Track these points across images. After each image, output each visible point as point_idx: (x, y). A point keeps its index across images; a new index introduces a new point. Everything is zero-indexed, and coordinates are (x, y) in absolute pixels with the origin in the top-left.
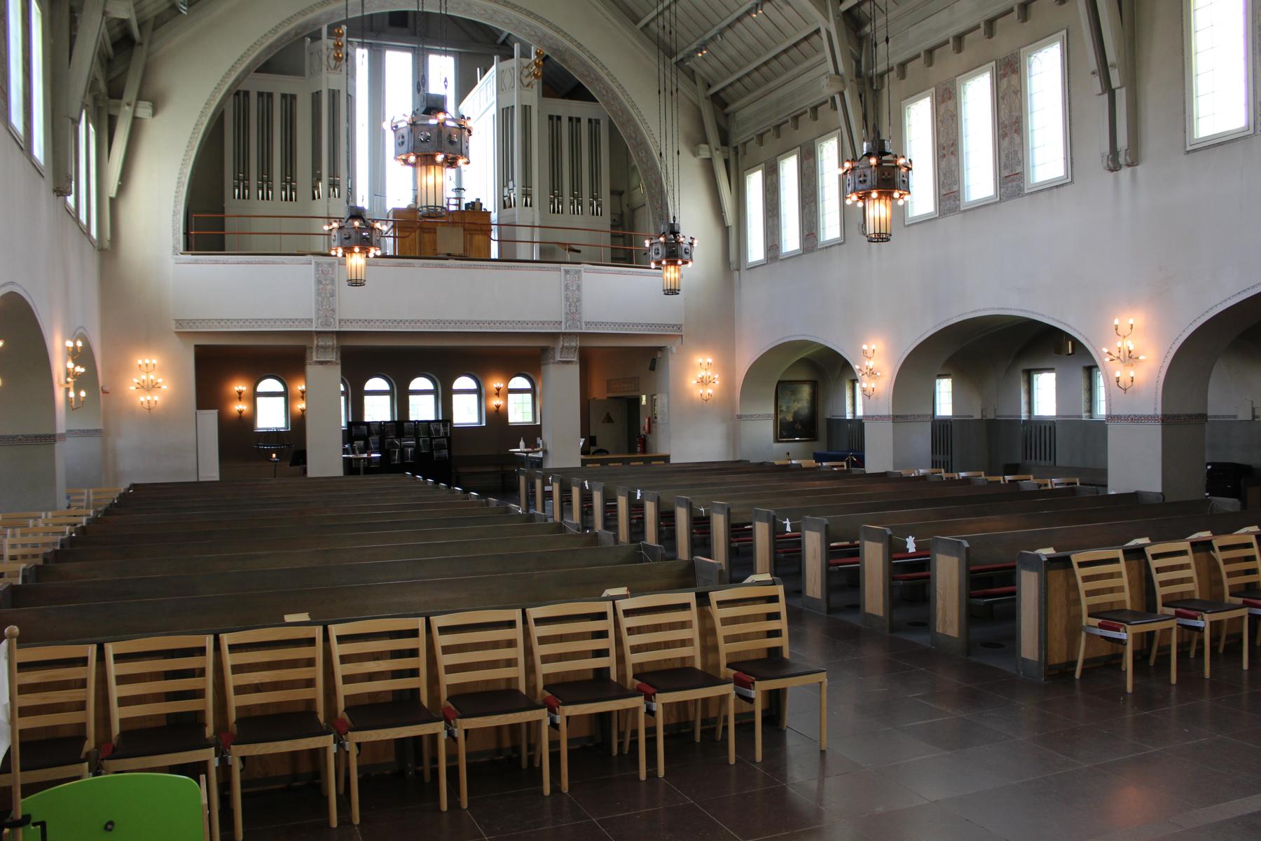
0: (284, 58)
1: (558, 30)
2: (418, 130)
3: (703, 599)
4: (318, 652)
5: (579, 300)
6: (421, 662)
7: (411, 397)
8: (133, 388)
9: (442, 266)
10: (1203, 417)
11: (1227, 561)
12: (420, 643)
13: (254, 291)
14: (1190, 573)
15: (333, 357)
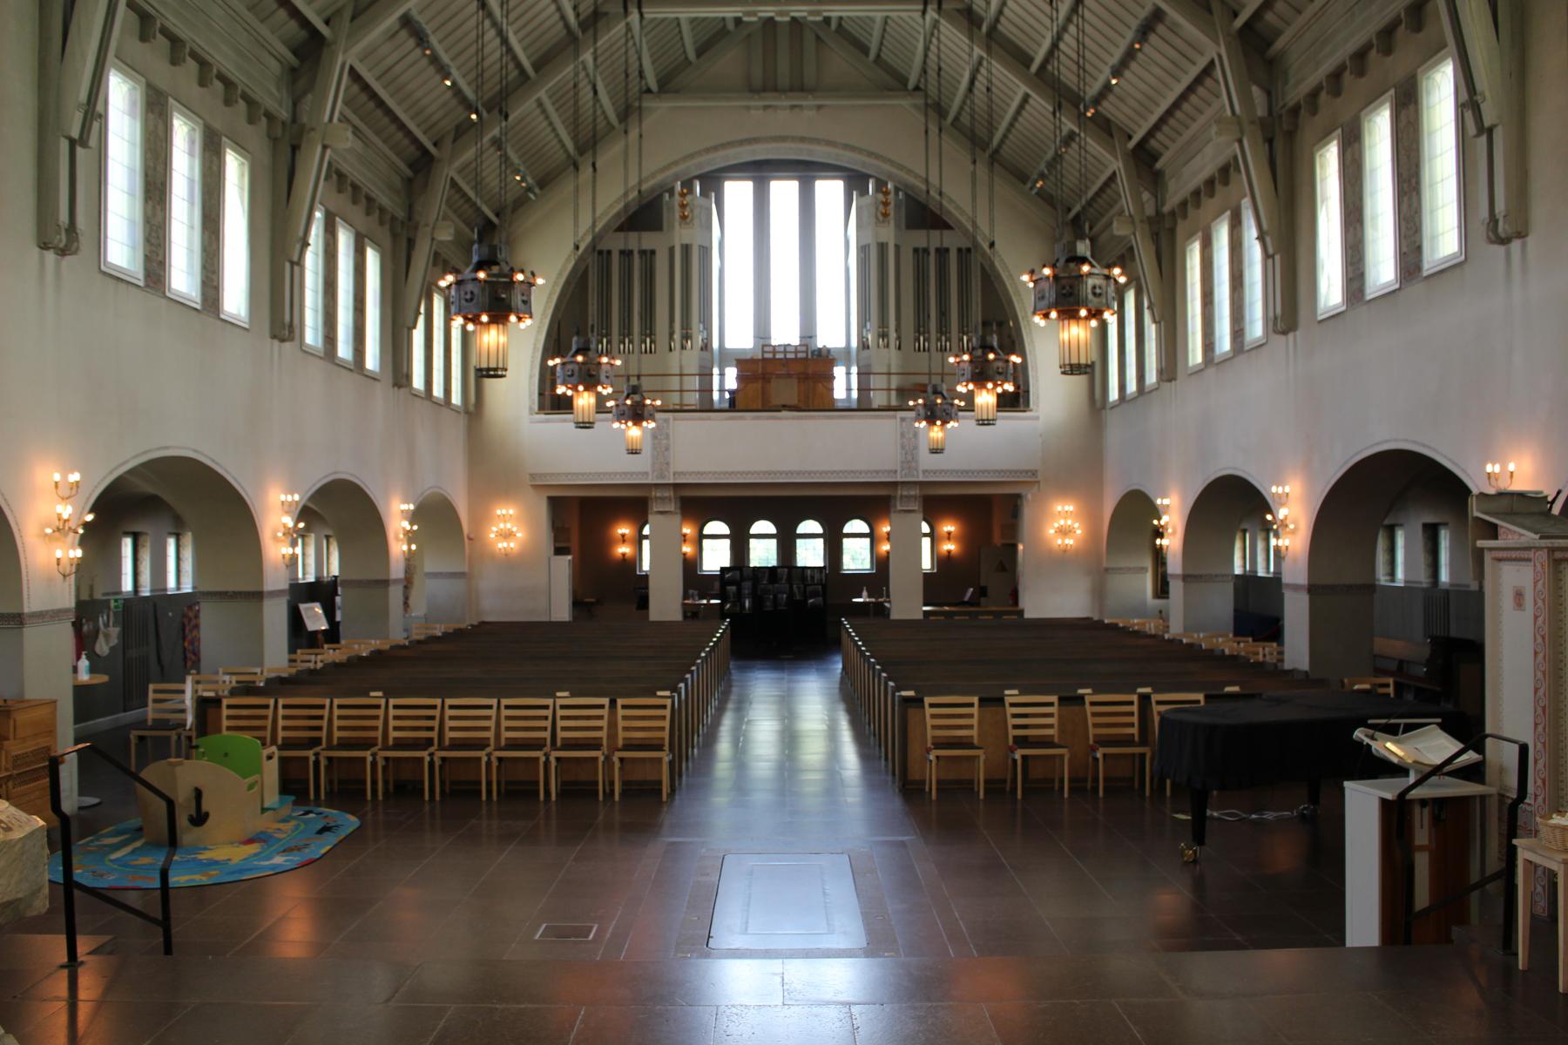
0: (645, 214)
1: (901, 167)
2: (785, 262)
3: (613, 703)
4: (381, 712)
5: (916, 448)
6: (436, 724)
7: (845, 541)
8: (1052, 531)
10: (1371, 588)
11: (1094, 714)
12: (437, 713)
13: (603, 445)
15: (671, 507)
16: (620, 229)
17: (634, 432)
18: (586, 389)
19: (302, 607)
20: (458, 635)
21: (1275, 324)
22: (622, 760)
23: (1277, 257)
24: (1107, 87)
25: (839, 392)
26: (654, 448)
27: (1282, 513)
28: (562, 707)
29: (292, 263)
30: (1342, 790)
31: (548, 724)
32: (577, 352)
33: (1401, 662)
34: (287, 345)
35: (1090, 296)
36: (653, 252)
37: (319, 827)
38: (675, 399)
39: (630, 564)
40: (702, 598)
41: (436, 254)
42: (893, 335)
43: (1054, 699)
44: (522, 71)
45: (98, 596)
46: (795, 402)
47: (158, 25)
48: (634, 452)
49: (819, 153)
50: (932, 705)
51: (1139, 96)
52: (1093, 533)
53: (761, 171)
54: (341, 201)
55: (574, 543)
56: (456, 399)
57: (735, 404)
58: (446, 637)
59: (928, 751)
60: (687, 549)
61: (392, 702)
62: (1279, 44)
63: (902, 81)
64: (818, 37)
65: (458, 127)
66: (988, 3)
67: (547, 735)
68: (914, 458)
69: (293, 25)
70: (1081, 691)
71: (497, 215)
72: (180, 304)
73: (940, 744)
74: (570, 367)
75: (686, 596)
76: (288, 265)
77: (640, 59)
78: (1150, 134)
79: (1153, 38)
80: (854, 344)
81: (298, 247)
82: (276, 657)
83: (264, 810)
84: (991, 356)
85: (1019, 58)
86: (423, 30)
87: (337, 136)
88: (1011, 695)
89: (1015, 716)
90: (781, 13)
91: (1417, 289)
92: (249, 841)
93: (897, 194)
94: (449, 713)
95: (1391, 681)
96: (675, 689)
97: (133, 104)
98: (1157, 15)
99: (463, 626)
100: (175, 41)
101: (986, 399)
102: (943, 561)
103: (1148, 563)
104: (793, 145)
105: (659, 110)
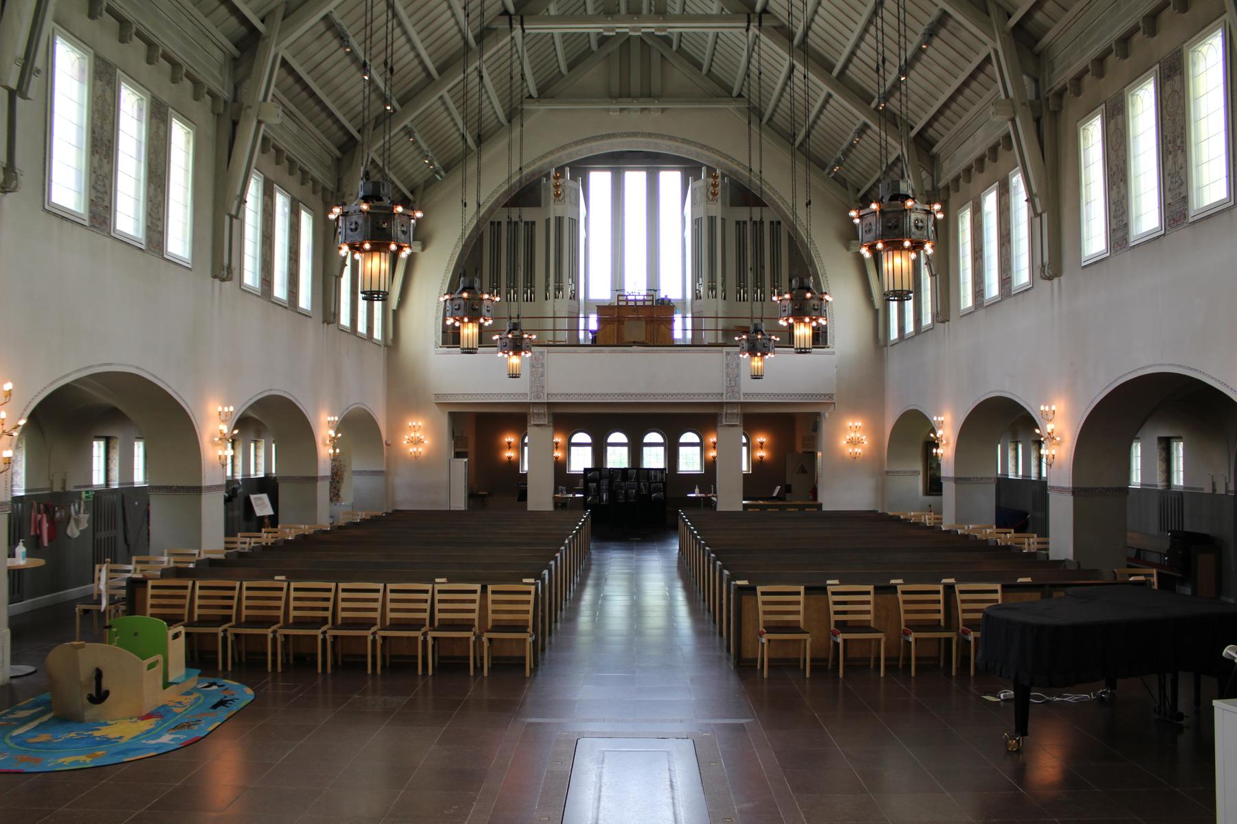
0: (527, 194)
1: (727, 157)
2: (636, 233)
3: (484, 588)
4: (283, 594)
5: (738, 376)
6: (330, 604)
7: (646, 450)
9: (626, 352)
11: (905, 602)
12: (331, 595)
13: (493, 376)
14: (869, 607)
15: (545, 421)
16: (505, 206)
17: (514, 360)
18: (470, 321)
19: (252, 497)
20: (374, 521)
21: (1043, 271)
22: (490, 640)
23: (1045, 216)
24: (852, 145)
25: (678, 334)
26: (532, 374)
27: (940, 433)
28: (440, 592)
29: (231, 217)
30: (1211, 709)
31: (427, 606)
32: (464, 290)
33: (1139, 550)
34: (227, 283)
35: (913, 229)
36: (533, 223)
37: (216, 701)
38: (549, 336)
39: (514, 465)
40: (568, 493)
41: (265, 139)
42: (719, 288)
43: (870, 588)
44: (429, 74)
45: (70, 488)
46: (642, 339)
47: (105, 4)
48: (514, 376)
49: (663, 147)
50: (763, 593)
51: (922, 93)
52: (877, 444)
53: (617, 162)
54: (279, 172)
55: (471, 449)
56: (377, 335)
57: (597, 341)
58: (364, 522)
59: (761, 634)
60: (558, 454)
61: (293, 585)
62: (1047, 39)
63: (729, 90)
64: (662, 56)
65: (377, 118)
66: (805, 4)
67: (426, 616)
68: (737, 385)
69: (233, 21)
70: (893, 581)
71: (412, 192)
72: (125, 242)
73: (772, 628)
74: (457, 302)
75: (556, 491)
76: (227, 218)
77: (521, 64)
78: (929, 124)
79: (936, 42)
80: (689, 296)
81: (236, 203)
82: (213, 539)
83: (166, 684)
84: (809, 295)
85: (825, 66)
86: (344, 31)
87: (268, 112)
88: (833, 584)
89: (836, 603)
90: (634, 29)
91: (1183, 233)
92: (149, 716)
93: (723, 178)
94: (341, 595)
95: (1155, 571)
96: (538, 576)
97: (82, 70)
98: (944, 17)
99: (379, 513)
100: (123, 22)
101: (803, 332)
102: (757, 465)
103: (919, 467)
104: (643, 140)
105: (538, 111)
